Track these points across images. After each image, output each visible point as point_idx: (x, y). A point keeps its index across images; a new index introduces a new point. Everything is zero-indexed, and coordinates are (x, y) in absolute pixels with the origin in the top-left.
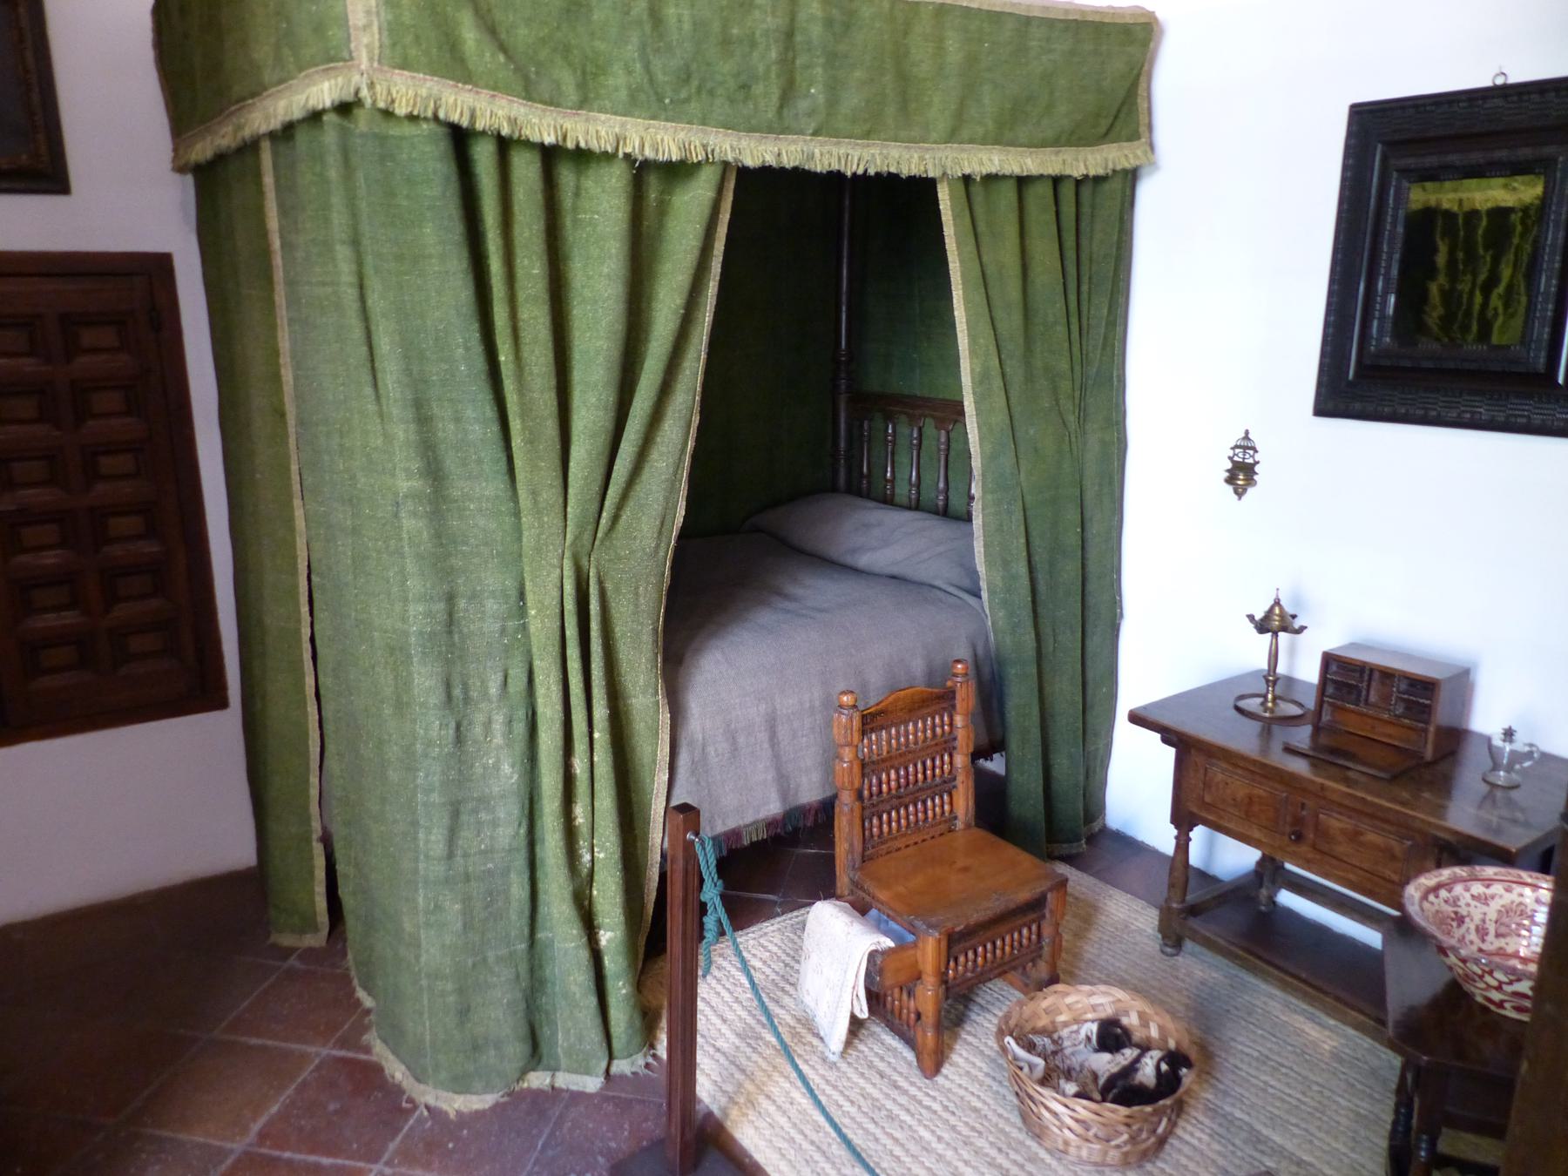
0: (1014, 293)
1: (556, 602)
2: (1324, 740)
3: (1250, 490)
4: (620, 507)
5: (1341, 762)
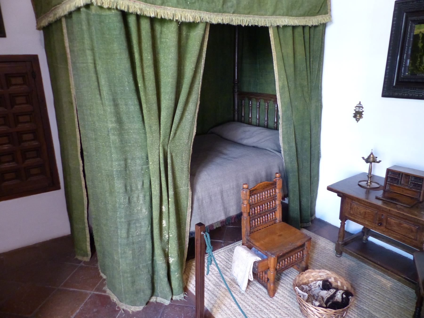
0: (292, 62)
1: (157, 160)
2: (387, 195)
3: (361, 120)
4: (176, 130)
5: (394, 202)
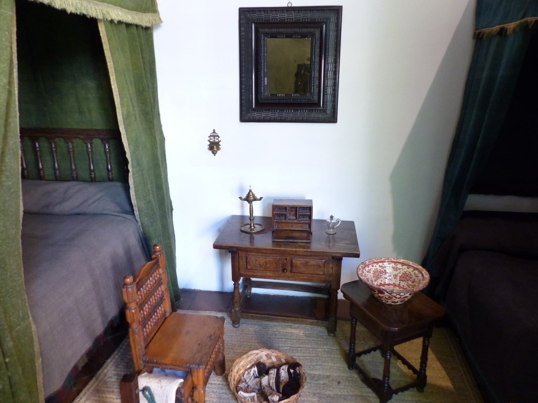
3: (218, 152)
